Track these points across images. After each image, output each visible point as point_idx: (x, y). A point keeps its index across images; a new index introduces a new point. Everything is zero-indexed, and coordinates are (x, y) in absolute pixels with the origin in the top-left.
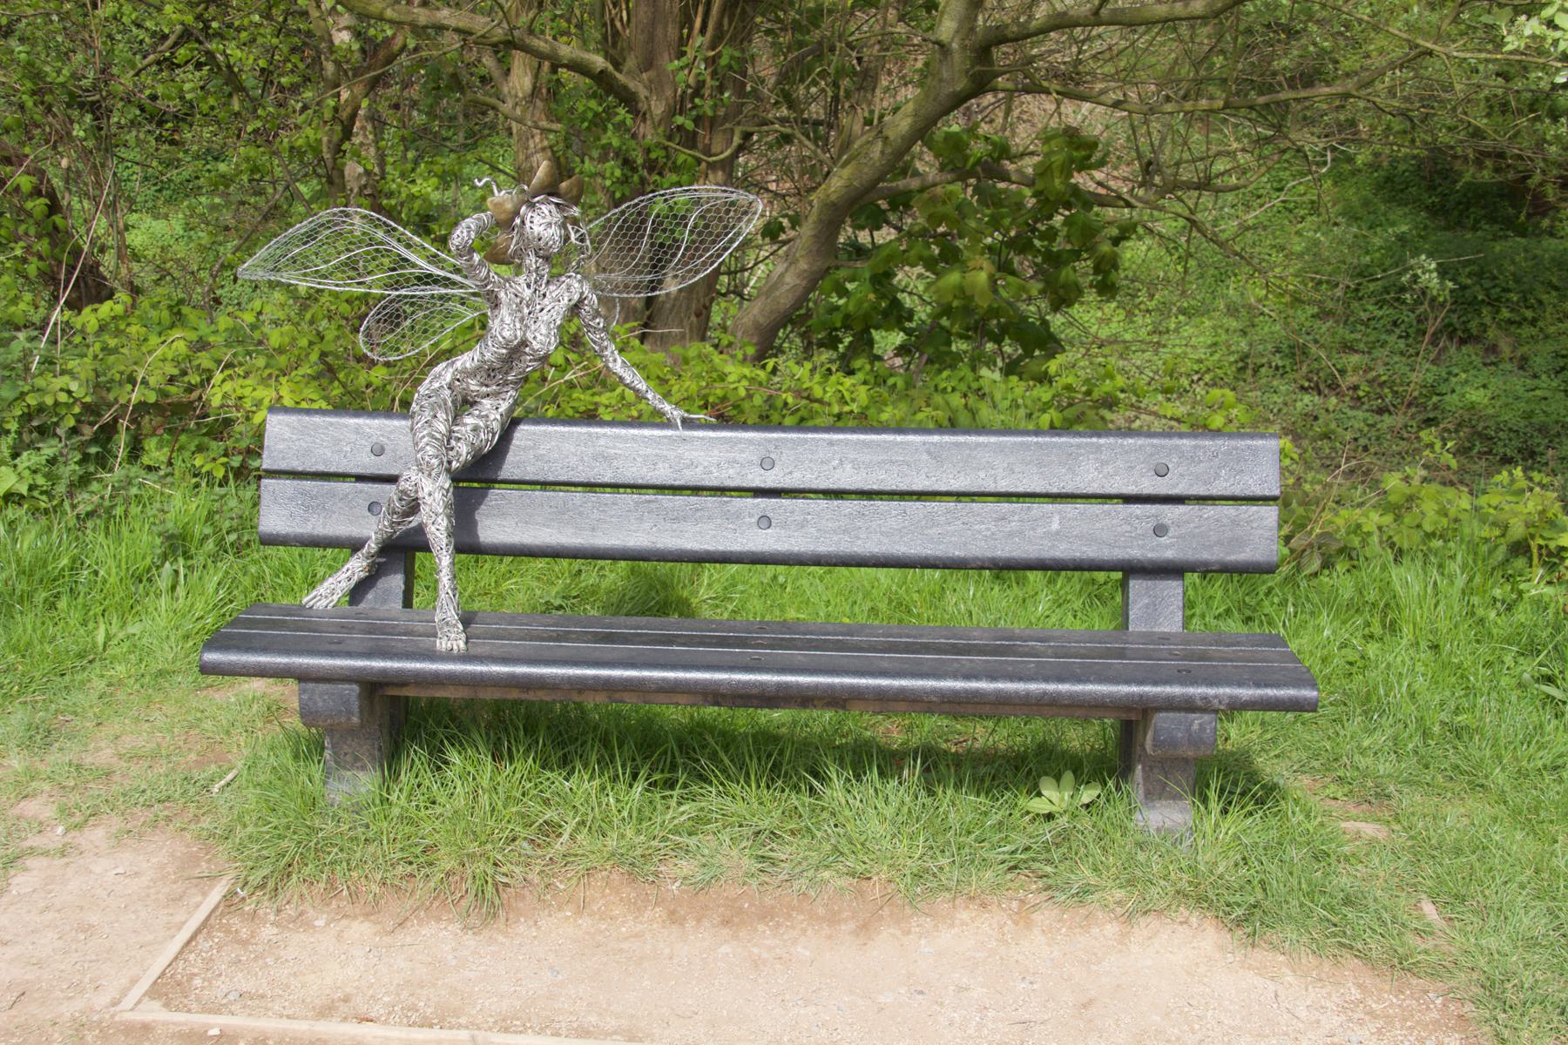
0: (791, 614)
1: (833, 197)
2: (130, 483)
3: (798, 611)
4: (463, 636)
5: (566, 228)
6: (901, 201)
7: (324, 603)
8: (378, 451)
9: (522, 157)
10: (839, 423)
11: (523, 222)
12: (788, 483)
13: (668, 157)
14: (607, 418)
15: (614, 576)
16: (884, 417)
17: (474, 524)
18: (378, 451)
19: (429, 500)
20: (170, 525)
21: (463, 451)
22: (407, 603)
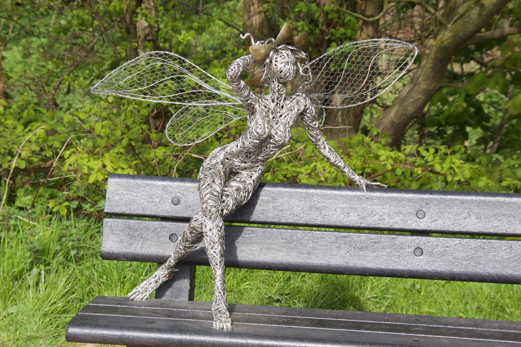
0: (425, 309)
1: (446, 43)
2: (10, 218)
3: (429, 307)
4: (230, 320)
5: (297, 65)
6: (485, 45)
7: (140, 296)
8: (176, 202)
9: (246, 17)
10: (447, 189)
11: (271, 62)
12: (433, 227)
13: (339, 18)
14: (304, 181)
15: (310, 282)
16: (481, 184)
17: (235, 248)
18: (176, 202)
19: (209, 234)
20: (36, 244)
21: (230, 203)
22: (191, 297)
